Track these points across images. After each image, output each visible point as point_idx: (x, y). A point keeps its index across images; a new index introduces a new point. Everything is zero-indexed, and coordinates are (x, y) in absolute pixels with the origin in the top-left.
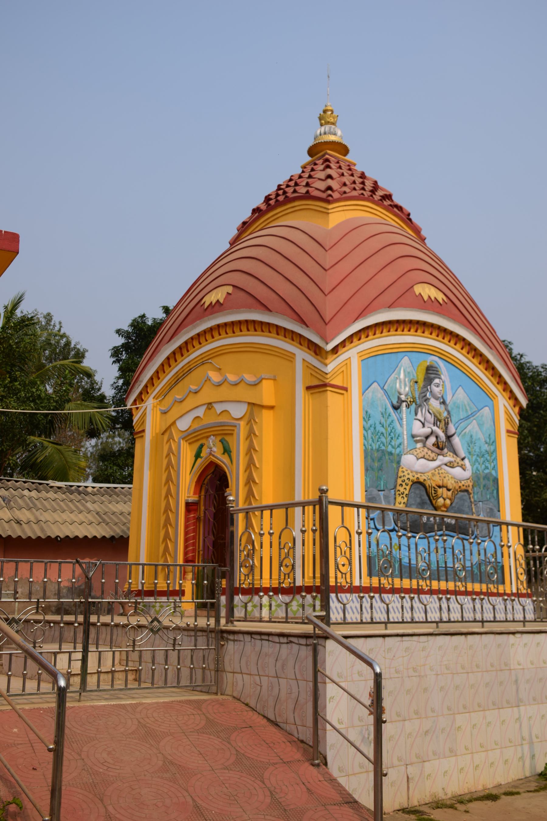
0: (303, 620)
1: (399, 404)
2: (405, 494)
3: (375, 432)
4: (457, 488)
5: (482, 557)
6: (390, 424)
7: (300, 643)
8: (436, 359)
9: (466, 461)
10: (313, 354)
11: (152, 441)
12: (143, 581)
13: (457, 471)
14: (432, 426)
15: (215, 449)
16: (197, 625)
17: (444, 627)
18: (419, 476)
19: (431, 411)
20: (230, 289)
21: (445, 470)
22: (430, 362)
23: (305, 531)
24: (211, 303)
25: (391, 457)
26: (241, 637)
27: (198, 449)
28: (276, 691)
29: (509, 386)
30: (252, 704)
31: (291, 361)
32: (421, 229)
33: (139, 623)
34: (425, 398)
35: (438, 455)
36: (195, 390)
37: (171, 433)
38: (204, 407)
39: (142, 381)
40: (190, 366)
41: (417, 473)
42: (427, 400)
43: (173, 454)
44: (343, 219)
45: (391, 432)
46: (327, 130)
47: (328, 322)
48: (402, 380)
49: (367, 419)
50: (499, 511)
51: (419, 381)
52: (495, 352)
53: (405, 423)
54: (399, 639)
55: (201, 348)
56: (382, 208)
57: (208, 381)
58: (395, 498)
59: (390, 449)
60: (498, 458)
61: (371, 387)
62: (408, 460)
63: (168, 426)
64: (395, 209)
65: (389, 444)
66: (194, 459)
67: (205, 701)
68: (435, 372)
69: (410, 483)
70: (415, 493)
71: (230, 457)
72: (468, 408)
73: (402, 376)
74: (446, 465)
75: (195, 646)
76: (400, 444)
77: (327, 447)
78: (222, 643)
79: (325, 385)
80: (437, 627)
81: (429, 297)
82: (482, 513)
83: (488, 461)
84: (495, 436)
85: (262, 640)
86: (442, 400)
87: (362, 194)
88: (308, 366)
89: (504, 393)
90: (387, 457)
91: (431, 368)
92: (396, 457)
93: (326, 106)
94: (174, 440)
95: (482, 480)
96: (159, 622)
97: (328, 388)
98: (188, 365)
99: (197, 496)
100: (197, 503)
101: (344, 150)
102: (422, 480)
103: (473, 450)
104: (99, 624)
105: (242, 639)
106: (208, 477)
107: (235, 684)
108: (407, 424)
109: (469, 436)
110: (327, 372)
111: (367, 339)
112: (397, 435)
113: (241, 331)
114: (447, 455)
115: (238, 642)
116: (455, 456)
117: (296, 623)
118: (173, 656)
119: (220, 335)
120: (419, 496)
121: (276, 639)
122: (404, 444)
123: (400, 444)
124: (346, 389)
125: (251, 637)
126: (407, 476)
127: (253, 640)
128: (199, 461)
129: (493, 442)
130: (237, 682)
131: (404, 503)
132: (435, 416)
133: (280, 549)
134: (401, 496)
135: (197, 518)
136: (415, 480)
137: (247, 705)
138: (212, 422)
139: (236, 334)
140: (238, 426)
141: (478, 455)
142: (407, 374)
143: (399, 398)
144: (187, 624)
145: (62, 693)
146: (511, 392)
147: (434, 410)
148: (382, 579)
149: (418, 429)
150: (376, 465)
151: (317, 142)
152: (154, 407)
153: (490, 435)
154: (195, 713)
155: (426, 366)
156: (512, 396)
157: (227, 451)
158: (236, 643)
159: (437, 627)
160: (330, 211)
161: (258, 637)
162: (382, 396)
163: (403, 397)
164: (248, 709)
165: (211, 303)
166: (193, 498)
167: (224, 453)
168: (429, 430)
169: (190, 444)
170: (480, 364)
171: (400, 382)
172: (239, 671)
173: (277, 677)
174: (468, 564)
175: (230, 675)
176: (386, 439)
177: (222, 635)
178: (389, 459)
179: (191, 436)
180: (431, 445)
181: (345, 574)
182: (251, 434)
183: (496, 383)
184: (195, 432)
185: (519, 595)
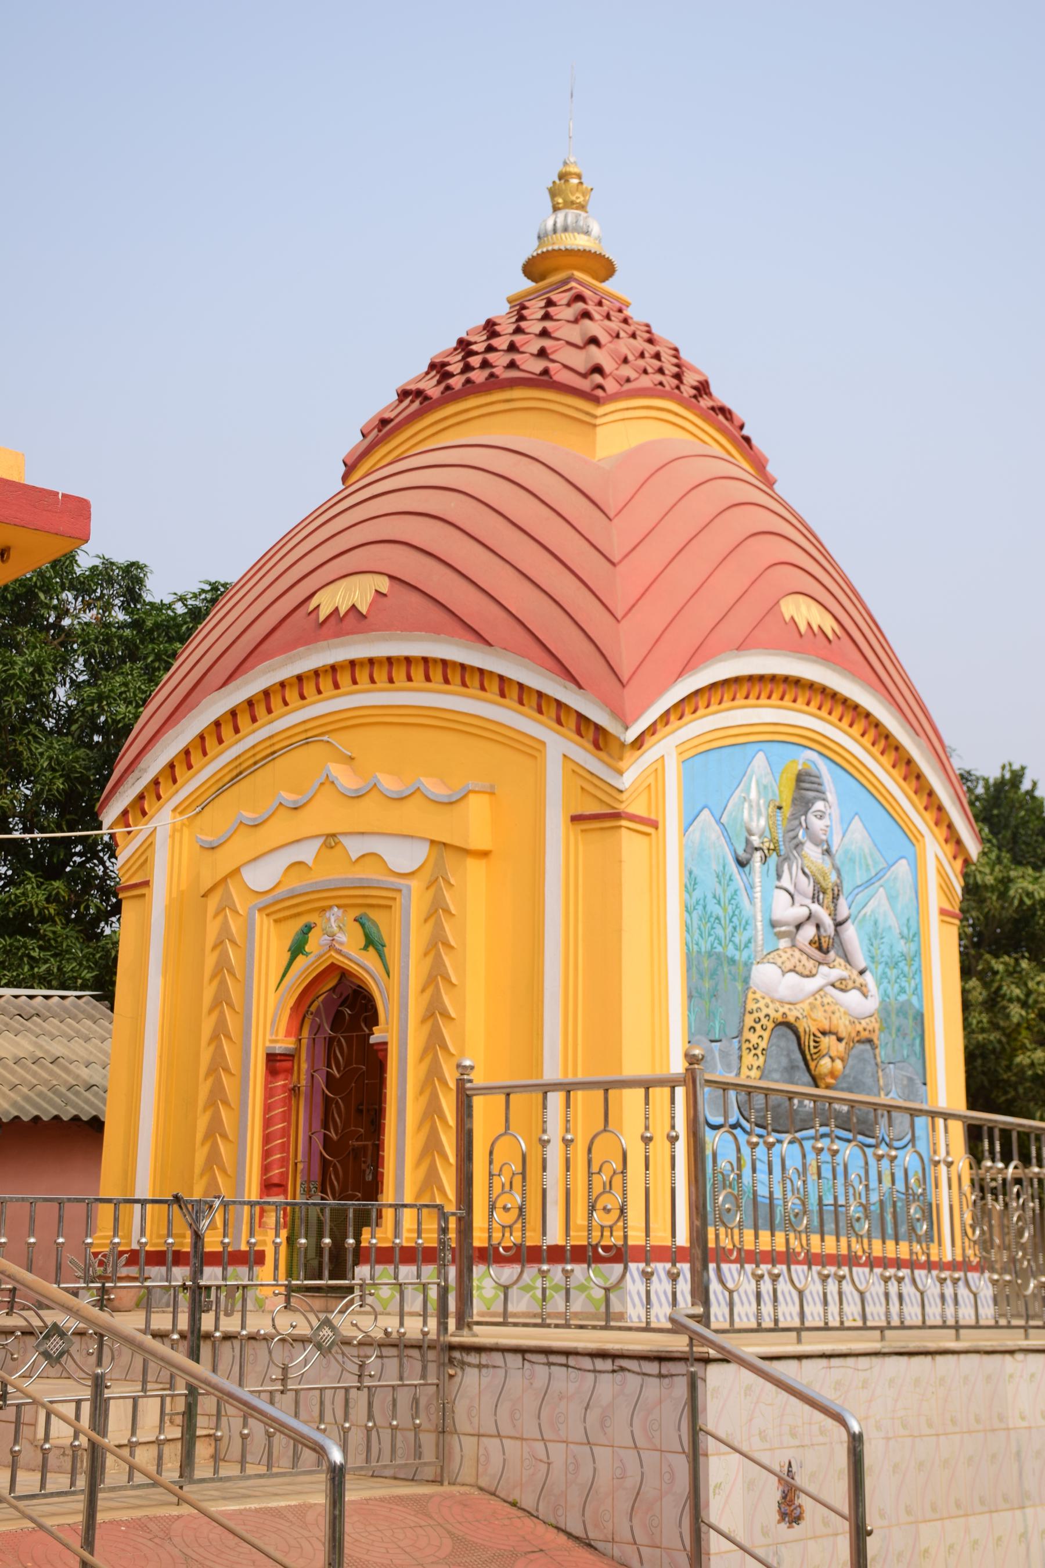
0: (543, 1319)
1: (747, 856)
2: (760, 1049)
3: (707, 917)
4: (854, 1034)
5: (900, 1186)
6: (732, 898)
7: (644, 1371)
8: (814, 756)
9: (869, 978)
10: (591, 747)
11: (169, 909)
12: (226, 1240)
13: (853, 998)
14: (808, 902)
15: (342, 937)
16: (404, 1334)
17: (897, 1340)
18: (785, 1009)
19: (807, 870)
20: (383, 584)
21: (832, 996)
22: (804, 763)
23: (650, 1139)
24: (337, 609)
25: (733, 969)
26: (497, 1358)
27: (297, 934)
28: (586, 1473)
29: (947, 814)
30: (528, 1503)
31: (535, 757)
32: (767, 461)
33: (295, 1332)
34: (795, 842)
35: (820, 963)
36: (294, 802)
37: (228, 896)
38: (318, 843)
39: (145, 770)
40: (273, 744)
41: (782, 1002)
42: (799, 845)
43: (233, 942)
44: (634, 443)
45: (734, 915)
46: (570, 220)
47: (628, 682)
48: (754, 804)
49: (690, 888)
50: (925, 1084)
51: (784, 804)
52: (923, 741)
53: (758, 895)
54: (824, 1362)
55: (304, 707)
56: (696, 415)
57: (327, 786)
58: (740, 1057)
59: (731, 951)
60: (923, 969)
61: (698, 819)
62: (768, 977)
63: (219, 878)
64: (721, 417)
65: (730, 941)
66: (287, 956)
67: (430, 1497)
68: (816, 786)
69: (770, 1025)
70: (778, 1046)
71: (381, 956)
72: (870, 862)
73: (753, 795)
74: (833, 985)
75: (401, 1378)
76: (749, 941)
77: (620, 949)
78: (452, 1372)
79: (617, 816)
80: (883, 1338)
81: (809, 624)
82: (894, 1088)
83: (905, 976)
84: (918, 922)
85: (550, 1364)
86: (825, 847)
87: (661, 384)
88: (574, 769)
89: (936, 830)
90: (726, 970)
91: (807, 778)
92: (741, 968)
93: (565, 164)
94: (235, 911)
95: (893, 1017)
96: (333, 1328)
97: (624, 823)
98: (268, 743)
99: (293, 1039)
100: (293, 1056)
101: (605, 268)
102: (791, 1019)
103: (879, 952)
104: (217, 1334)
105: (501, 1363)
106: (321, 999)
107: (482, 1459)
108: (763, 899)
109: (872, 923)
110: (621, 787)
111: (694, 716)
112: (743, 922)
113: (409, 679)
114: (836, 963)
115: (491, 1370)
116: (848, 967)
117: (594, 1327)
118: (359, 1399)
119: (355, 682)
120: (785, 1053)
121: (586, 1363)
122: (756, 942)
123: (749, 941)
124: (655, 824)
125: (524, 1359)
126: (765, 1011)
127: (527, 1365)
128: (301, 961)
129: (915, 935)
130: (487, 1456)
131: (759, 1067)
132: (816, 883)
133: (590, 1174)
134: (753, 1052)
135: (293, 1089)
136: (780, 1019)
137: (514, 1504)
138: (336, 876)
139: (397, 685)
140: (405, 891)
141: (887, 964)
142: (763, 789)
143: (748, 842)
144: (386, 1332)
145: (337, 1476)
146: (950, 826)
147: (813, 868)
148: (792, 1235)
149: (786, 911)
150: (707, 985)
151: (545, 250)
152: (174, 830)
153: (908, 920)
154: (423, 1523)
155: (796, 772)
156: (953, 839)
157: (372, 942)
158: (484, 1371)
159: (883, 1338)
160: (598, 421)
161: (542, 1358)
162: (718, 838)
163: (756, 841)
164: (520, 1513)
165: (337, 609)
166: (284, 1044)
167: (365, 948)
168: (804, 912)
169: (276, 921)
170: (894, 766)
171: (751, 806)
172: (494, 1432)
173: (589, 1443)
174: (874, 1198)
175: (469, 1443)
176: (724, 929)
177: (453, 1354)
178: (730, 973)
179: (279, 906)
180: (807, 943)
181: (732, 1229)
182: (437, 909)
183: (921, 808)
184: (292, 897)
185: (965, 1265)
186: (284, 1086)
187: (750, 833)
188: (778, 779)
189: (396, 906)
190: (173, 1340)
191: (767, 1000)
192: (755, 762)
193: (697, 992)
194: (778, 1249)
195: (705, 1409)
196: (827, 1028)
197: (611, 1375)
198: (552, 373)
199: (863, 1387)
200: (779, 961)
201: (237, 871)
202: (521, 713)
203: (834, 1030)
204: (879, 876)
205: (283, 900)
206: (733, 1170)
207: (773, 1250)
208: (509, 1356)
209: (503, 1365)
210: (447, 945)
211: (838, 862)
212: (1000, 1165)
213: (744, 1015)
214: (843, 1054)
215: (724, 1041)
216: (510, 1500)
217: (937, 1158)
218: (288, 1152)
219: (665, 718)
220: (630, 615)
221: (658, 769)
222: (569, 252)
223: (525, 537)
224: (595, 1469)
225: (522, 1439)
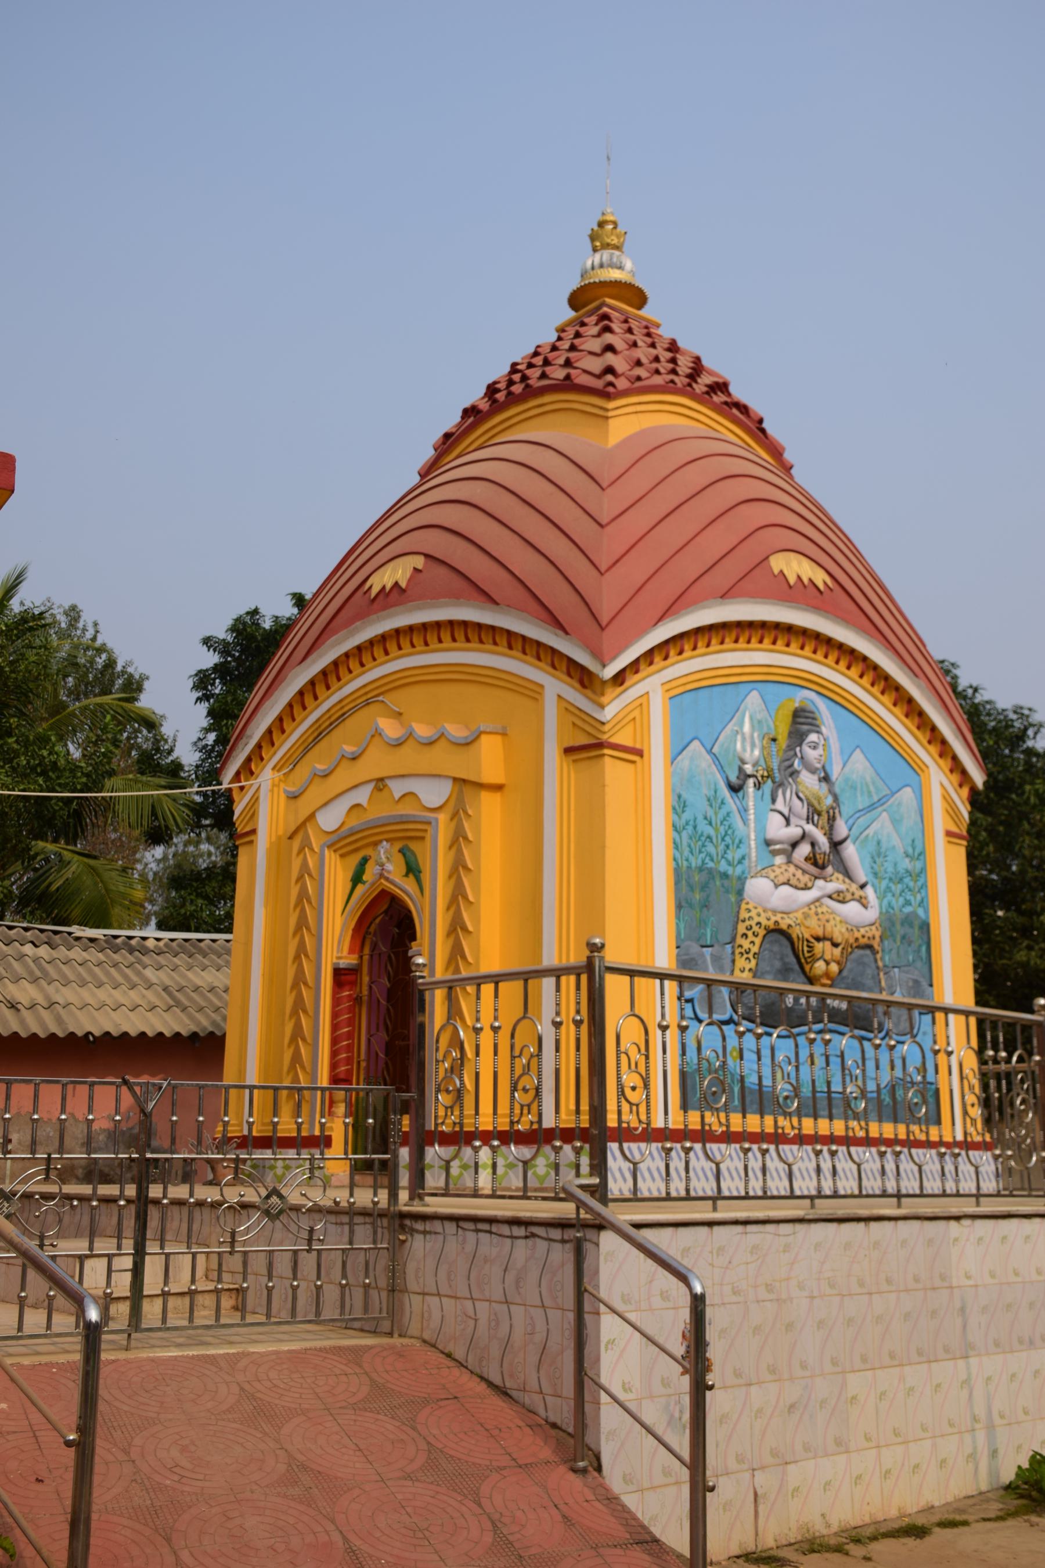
0: (556, 1193)
1: (740, 782)
3: (696, 836)
4: (852, 941)
6: (725, 819)
8: (812, 695)
9: (869, 891)
10: (577, 685)
11: (269, 851)
13: (852, 909)
14: (803, 823)
15: (389, 867)
16: (354, 1203)
17: (825, 1207)
18: (778, 918)
19: (801, 795)
20: (419, 562)
21: (828, 907)
22: (801, 701)
24: (384, 587)
25: (726, 882)
26: (437, 1226)
28: (504, 1329)
29: (950, 747)
30: (460, 1354)
31: (536, 699)
32: (784, 449)
33: (243, 1199)
34: (790, 770)
35: (816, 878)
36: (353, 753)
37: (307, 837)
38: (370, 787)
39: (250, 737)
41: (775, 912)
42: (794, 774)
43: (310, 875)
45: (726, 834)
47: (607, 625)
49: (679, 810)
50: (931, 985)
51: (780, 737)
52: (923, 683)
53: (752, 817)
54: (739, 1228)
55: (364, 673)
56: (709, 408)
58: (733, 961)
59: (723, 866)
62: (758, 887)
64: (735, 411)
65: (723, 857)
66: (349, 885)
67: (370, 1348)
68: (810, 720)
70: (771, 951)
71: (419, 881)
72: (872, 788)
73: (747, 728)
74: (830, 897)
75: (351, 1243)
76: (743, 858)
78: (402, 1237)
79: (600, 745)
80: (813, 1206)
81: (799, 578)
82: (898, 989)
83: (910, 890)
84: (924, 843)
85: (477, 1231)
86: (822, 775)
87: (672, 381)
88: (567, 708)
89: (941, 762)
90: (718, 883)
91: (802, 714)
92: (734, 882)
93: (603, 214)
94: (312, 849)
95: (898, 926)
96: (281, 1197)
97: (606, 751)
98: (338, 707)
99: (356, 956)
101: (639, 298)
103: (882, 869)
104: (165, 1201)
105: (440, 1230)
106: (377, 921)
107: (426, 1315)
109: (875, 843)
110: (603, 720)
111: (680, 657)
112: (737, 841)
113: (440, 641)
114: (833, 878)
115: (433, 1236)
116: (847, 880)
118: (307, 1263)
120: (778, 957)
121: (505, 1230)
122: (750, 859)
123: (743, 858)
124: (640, 753)
125: (458, 1226)
126: (756, 919)
127: (460, 1231)
128: (360, 889)
129: (919, 854)
131: (750, 970)
132: (810, 804)
134: (745, 956)
135: (356, 999)
136: (772, 927)
137: (449, 1355)
138: (384, 814)
139: (432, 647)
140: (434, 824)
141: (891, 879)
143: (741, 770)
144: (335, 1202)
146: (955, 758)
147: (807, 793)
149: (777, 829)
150: (698, 897)
152: (274, 785)
153: (913, 841)
155: (792, 709)
156: (957, 767)
157: (412, 869)
158: (428, 1236)
159: (813, 1206)
160: (610, 414)
161: (470, 1226)
163: (748, 768)
164: (452, 1364)
165: (384, 587)
166: (348, 960)
167: (407, 875)
168: (799, 832)
169: (342, 856)
170: (895, 705)
171: (744, 739)
172: (435, 1291)
174: (871, 1086)
175: (416, 1299)
176: (716, 847)
178: (723, 886)
180: (802, 860)
181: (637, 1105)
182: (458, 837)
183: (925, 742)
184: (352, 834)
185: (968, 1145)
186: (349, 996)
187: (743, 762)
188: (773, 714)
189: (428, 837)
190: (120, 1206)
191: (760, 910)
192: (749, 699)
193: (687, 902)
194: (767, 1130)
195: (597, 1272)
196: (820, 933)
197: (524, 1241)
198: (573, 377)
199: (784, 1251)
200: (772, 875)
201: (312, 817)
202: (525, 662)
203: (828, 935)
204: (881, 801)
205: (345, 837)
206: (718, 1057)
207: (745, 1131)
208: (447, 1224)
209: (441, 1231)
210: (466, 868)
211: (837, 790)
212: (1003, 1054)
213: (737, 923)
214: (838, 958)
215: (716, 947)
216: (446, 1351)
217: (937, 1047)
218: (353, 1052)
219: (649, 656)
220: (614, 569)
221: (643, 703)
222: (603, 284)
223: (532, 511)
224: (511, 1326)
225: (456, 1298)
